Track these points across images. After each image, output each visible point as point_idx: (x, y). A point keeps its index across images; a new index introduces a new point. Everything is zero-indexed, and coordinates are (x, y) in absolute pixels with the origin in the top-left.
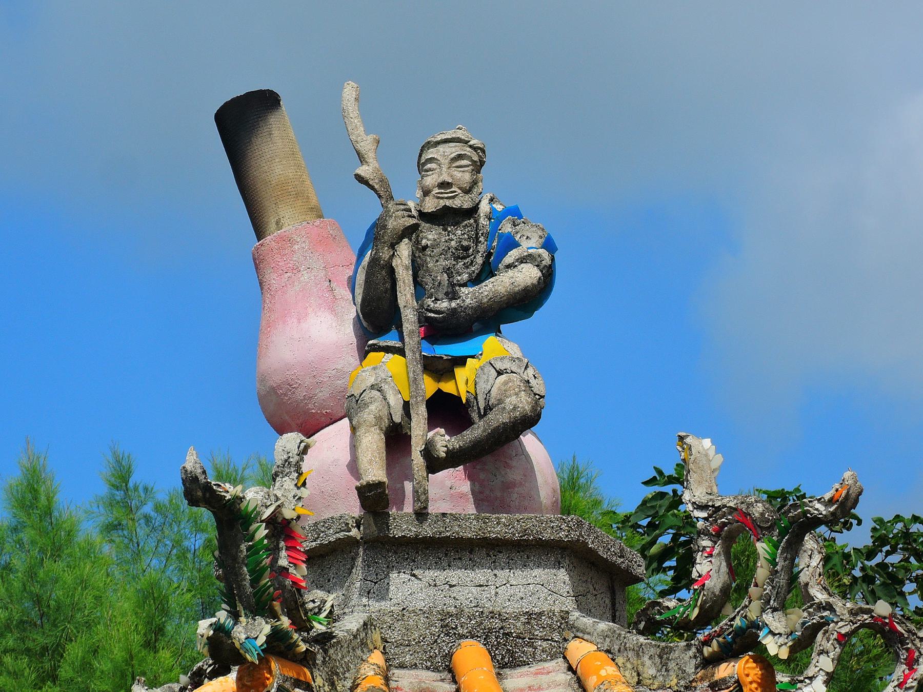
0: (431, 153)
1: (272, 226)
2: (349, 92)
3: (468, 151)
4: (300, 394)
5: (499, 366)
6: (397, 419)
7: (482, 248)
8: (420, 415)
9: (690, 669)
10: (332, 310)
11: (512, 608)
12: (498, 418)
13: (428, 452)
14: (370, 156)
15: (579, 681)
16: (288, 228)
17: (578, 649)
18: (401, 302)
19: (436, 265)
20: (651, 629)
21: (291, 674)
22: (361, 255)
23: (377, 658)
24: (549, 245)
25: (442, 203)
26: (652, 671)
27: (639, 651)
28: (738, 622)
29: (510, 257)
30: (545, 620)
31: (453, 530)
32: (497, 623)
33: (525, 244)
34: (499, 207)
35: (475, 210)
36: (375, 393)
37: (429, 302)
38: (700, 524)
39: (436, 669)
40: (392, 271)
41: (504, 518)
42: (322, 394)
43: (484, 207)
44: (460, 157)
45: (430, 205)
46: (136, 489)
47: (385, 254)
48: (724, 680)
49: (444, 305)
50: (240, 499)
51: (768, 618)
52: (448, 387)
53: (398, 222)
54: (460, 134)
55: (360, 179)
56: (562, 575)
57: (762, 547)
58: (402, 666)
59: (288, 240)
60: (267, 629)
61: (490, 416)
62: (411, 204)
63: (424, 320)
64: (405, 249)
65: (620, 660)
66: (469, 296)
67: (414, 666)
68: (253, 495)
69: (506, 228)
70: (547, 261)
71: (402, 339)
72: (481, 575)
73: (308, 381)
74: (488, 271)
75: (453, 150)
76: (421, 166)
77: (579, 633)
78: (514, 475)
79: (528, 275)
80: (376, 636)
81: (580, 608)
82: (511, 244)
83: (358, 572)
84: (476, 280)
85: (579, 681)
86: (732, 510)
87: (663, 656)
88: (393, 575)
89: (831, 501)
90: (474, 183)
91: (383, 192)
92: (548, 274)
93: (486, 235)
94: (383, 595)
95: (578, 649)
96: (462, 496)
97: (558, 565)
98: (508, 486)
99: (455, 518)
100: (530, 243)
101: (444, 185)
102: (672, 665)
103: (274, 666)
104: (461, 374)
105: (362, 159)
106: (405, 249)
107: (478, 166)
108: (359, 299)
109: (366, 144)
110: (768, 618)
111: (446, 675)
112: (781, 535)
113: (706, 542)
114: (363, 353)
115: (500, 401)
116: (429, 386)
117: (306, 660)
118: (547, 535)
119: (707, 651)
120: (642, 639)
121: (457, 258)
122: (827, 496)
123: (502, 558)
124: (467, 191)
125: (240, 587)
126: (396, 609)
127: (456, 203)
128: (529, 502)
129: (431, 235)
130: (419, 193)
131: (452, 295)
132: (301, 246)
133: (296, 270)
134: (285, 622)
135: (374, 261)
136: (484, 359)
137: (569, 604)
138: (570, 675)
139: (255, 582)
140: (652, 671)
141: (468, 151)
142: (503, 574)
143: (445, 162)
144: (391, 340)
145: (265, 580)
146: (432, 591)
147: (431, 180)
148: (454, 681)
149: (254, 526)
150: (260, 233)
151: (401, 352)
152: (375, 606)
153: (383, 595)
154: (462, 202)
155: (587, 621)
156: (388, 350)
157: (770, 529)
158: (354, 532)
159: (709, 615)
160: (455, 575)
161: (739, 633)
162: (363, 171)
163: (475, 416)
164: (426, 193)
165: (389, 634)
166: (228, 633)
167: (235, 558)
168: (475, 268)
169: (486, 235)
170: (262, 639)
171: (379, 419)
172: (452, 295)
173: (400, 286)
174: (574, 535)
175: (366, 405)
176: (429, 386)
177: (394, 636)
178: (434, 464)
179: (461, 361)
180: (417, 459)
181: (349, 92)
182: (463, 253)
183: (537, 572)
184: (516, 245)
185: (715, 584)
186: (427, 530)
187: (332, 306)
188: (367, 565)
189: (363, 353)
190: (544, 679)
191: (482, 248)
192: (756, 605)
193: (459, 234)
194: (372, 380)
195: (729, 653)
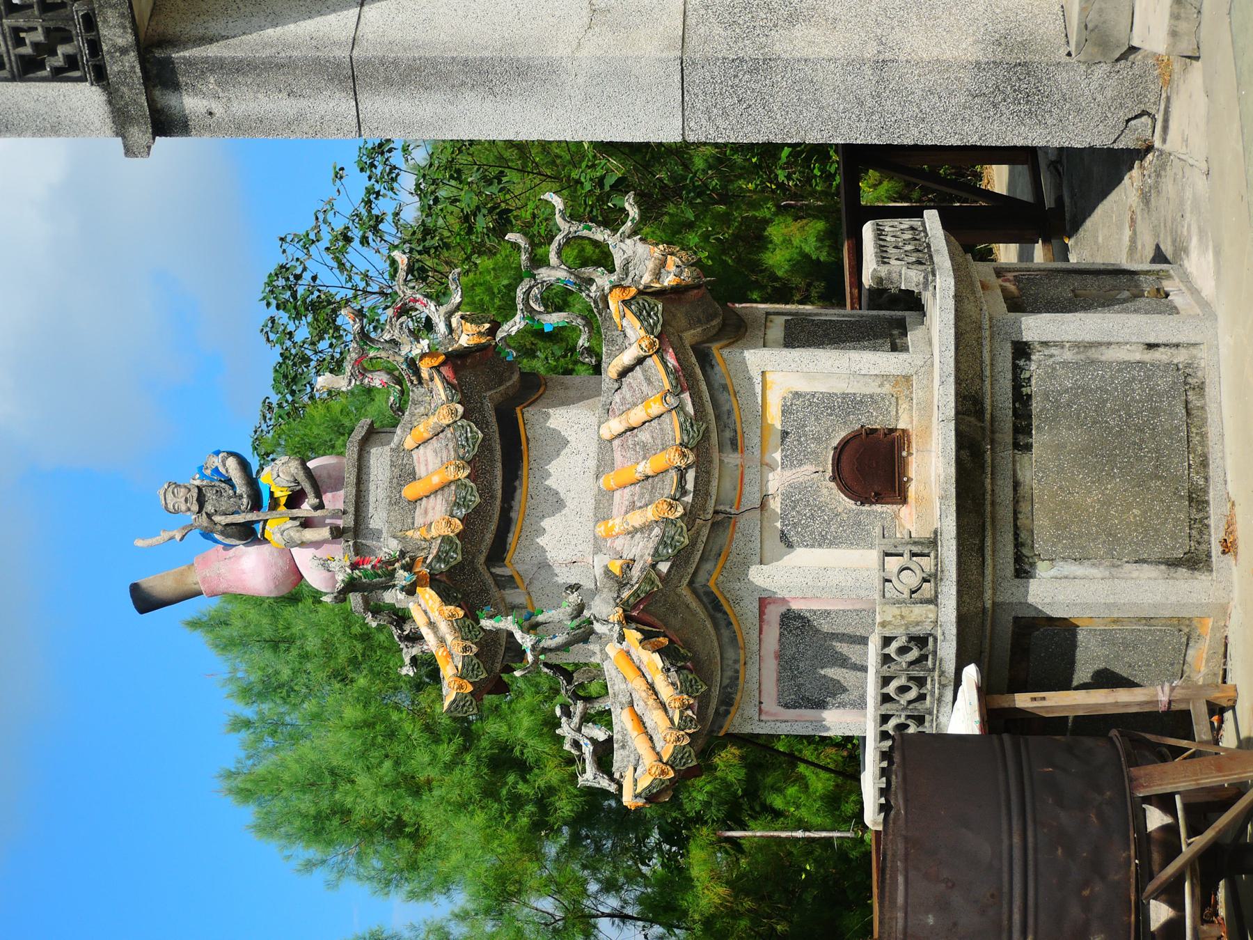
0: (170, 507)
1: (196, 586)
2: (139, 543)
3: (170, 489)
4: (280, 573)
5: (275, 476)
6: (297, 523)
7: (217, 483)
8: (296, 512)
9: (422, 390)
10: (241, 557)
11: (388, 474)
12: (301, 476)
13: (316, 508)
14: (171, 534)
15: (424, 443)
16: (198, 579)
17: (409, 443)
18: (242, 521)
19: (224, 504)
20: (401, 410)
21: (420, 564)
22: (216, 541)
23: (410, 533)
24: (217, 453)
25: (195, 502)
26: (422, 408)
27: (412, 415)
28: (404, 367)
29: (223, 472)
30: (394, 459)
31: (352, 498)
32: (395, 481)
33: (216, 464)
34: (198, 476)
35: (198, 487)
36: (285, 533)
37: (243, 508)
38: (358, 383)
39: (415, 508)
40: (227, 525)
41: (346, 475)
42: (280, 563)
43: (197, 483)
44: (173, 493)
45: (195, 508)
46: (237, 768)
47: (219, 528)
48: (429, 375)
49: (245, 501)
50: (343, 581)
51: (403, 353)
52: (283, 501)
53: (204, 520)
54: (162, 492)
55: (181, 539)
56: (373, 451)
57: (372, 354)
58: (413, 524)
59: (204, 580)
60: (401, 572)
61: (299, 480)
62: (193, 517)
63: (252, 510)
64: (217, 518)
65: (416, 424)
66: (241, 489)
67: (413, 518)
68: (340, 577)
69: (208, 472)
70: (225, 454)
71: (258, 521)
72: (372, 487)
73: (274, 569)
74: (228, 481)
75: (170, 496)
76: (176, 512)
77: (401, 443)
78: (324, 474)
79: (232, 463)
80: (400, 534)
81: (389, 443)
82: (216, 470)
83: (369, 543)
84: (233, 487)
85: (424, 443)
86: (353, 368)
87: (415, 403)
88: (371, 526)
89: (354, 321)
90: (185, 487)
91: (189, 528)
92: (231, 454)
93: (212, 481)
94: (380, 532)
95: (409, 443)
96: (333, 497)
97: (369, 452)
98: (330, 476)
99: (346, 497)
100: (216, 462)
101: (186, 500)
102: (420, 399)
103: (417, 570)
104: (277, 494)
105: (172, 538)
106: (217, 518)
107: (177, 486)
108: (238, 542)
109: (165, 535)
110: (403, 353)
111: (418, 504)
112: (367, 344)
113: (366, 381)
114: (265, 541)
115: (293, 475)
116: (282, 509)
117: (413, 559)
118: (356, 456)
119: (415, 382)
120: (407, 413)
121: (221, 495)
122: (352, 322)
123: (364, 477)
124: (190, 490)
125: (382, 583)
126: (387, 525)
127: (195, 495)
128: (340, 469)
129: (209, 508)
130: (189, 513)
131: (241, 497)
132: (207, 573)
133: (219, 575)
134: (397, 565)
135: (222, 533)
136: (271, 482)
137: (387, 448)
138: (421, 447)
139: (380, 576)
140: (422, 408)
141: (170, 489)
142: (372, 477)
143: (175, 500)
144: (259, 527)
145: (379, 572)
146: (379, 509)
147: (183, 508)
148: (421, 499)
149: (355, 575)
150: (200, 593)
151: (265, 521)
152: (385, 535)
153: (380, 532)
154: (195, 493)
155: (396, 439)
156: (264, 529)
157: (363, 350)
158: (351, 543)
159: (399, 381)
160: (372, 499)
161: (409, 366)
162: (178, 537)
163: (298, 488)
164: (189, 509)
165: (399, 529)
166: (404, 587)
167: (369, 585)
168: (227, 487)
169: (212, 481)
170: (406, 574)
171: (298, 531)
172: (241, 497)
173: (235, 521)
174: (356, 444)
175: (291, 537)
176: (282, 509)
177: (399, 526)
178: (320, 506)
179: (272, 493)
180: (319, 513)
181: (139, 543)
182: (219, 493)
183: (372, 462)
184: (217, 468)
185: (385, 377)
186: (351, 510)
187: (238, 557)
188: (366, 538)
189: (265, 541)
190: (422, 459)
191: (217, 483)
192: (398, 358)
193: (210, 495)
194: (279, 535)
195: (417, 372)
